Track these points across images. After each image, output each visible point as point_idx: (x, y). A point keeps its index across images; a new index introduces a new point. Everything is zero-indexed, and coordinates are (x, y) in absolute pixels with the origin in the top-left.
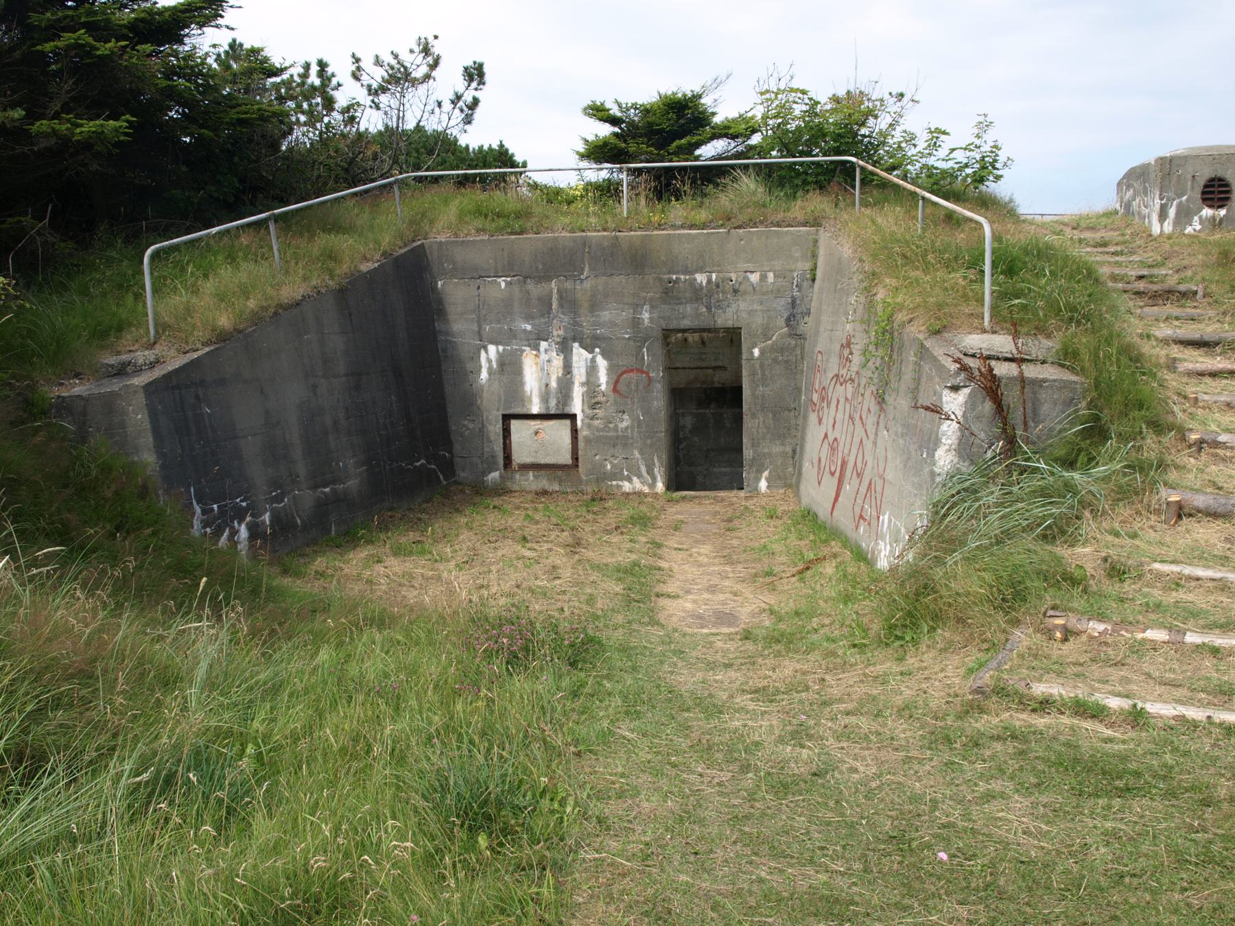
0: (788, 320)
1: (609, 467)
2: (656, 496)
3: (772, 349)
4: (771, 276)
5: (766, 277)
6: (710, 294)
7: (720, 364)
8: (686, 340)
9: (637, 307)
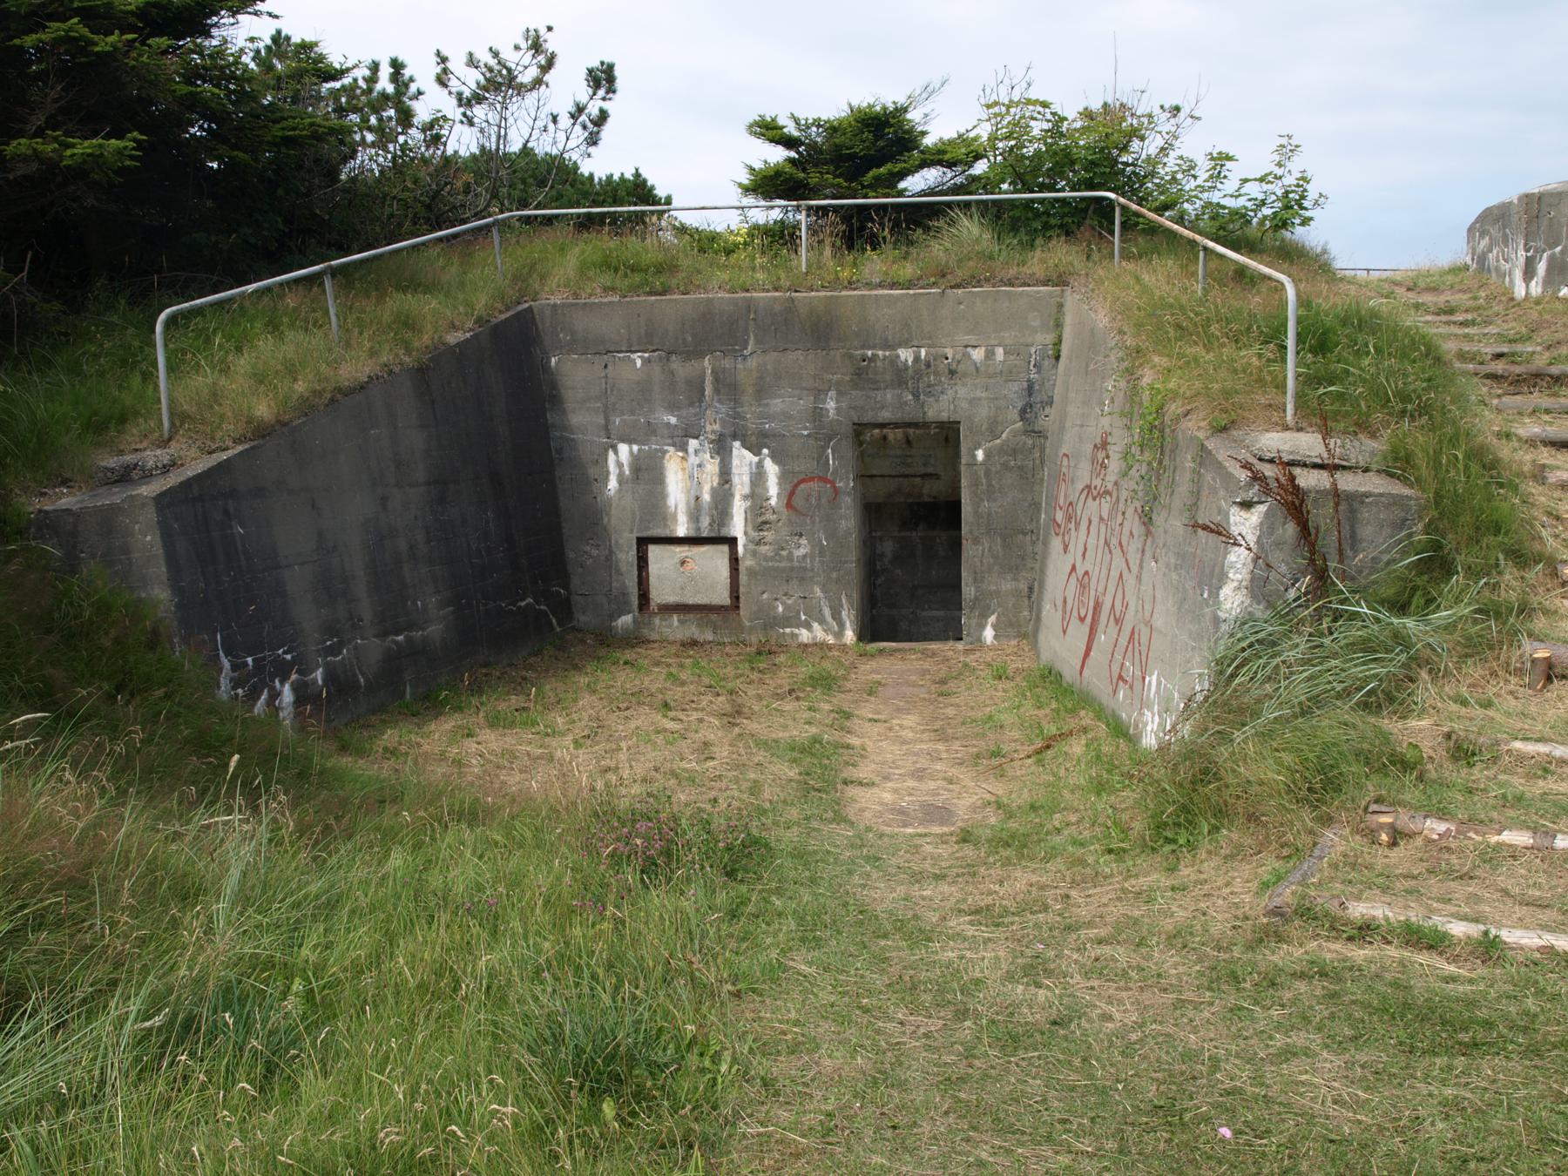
0: (1023, 412)
1: (781, 609)
2: (843, 648)
3: (1002, 450)
4: (1000, 352)
5: (993, 353)
6: (918, 375)
7: (930, 470)
8: (885, 438)
9: (819, 394)
